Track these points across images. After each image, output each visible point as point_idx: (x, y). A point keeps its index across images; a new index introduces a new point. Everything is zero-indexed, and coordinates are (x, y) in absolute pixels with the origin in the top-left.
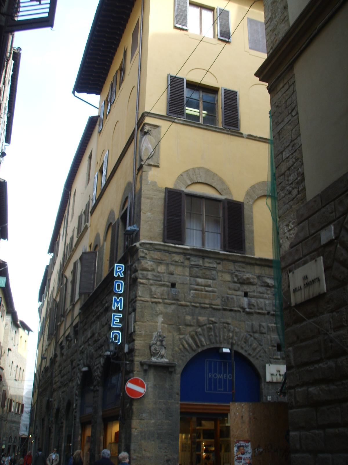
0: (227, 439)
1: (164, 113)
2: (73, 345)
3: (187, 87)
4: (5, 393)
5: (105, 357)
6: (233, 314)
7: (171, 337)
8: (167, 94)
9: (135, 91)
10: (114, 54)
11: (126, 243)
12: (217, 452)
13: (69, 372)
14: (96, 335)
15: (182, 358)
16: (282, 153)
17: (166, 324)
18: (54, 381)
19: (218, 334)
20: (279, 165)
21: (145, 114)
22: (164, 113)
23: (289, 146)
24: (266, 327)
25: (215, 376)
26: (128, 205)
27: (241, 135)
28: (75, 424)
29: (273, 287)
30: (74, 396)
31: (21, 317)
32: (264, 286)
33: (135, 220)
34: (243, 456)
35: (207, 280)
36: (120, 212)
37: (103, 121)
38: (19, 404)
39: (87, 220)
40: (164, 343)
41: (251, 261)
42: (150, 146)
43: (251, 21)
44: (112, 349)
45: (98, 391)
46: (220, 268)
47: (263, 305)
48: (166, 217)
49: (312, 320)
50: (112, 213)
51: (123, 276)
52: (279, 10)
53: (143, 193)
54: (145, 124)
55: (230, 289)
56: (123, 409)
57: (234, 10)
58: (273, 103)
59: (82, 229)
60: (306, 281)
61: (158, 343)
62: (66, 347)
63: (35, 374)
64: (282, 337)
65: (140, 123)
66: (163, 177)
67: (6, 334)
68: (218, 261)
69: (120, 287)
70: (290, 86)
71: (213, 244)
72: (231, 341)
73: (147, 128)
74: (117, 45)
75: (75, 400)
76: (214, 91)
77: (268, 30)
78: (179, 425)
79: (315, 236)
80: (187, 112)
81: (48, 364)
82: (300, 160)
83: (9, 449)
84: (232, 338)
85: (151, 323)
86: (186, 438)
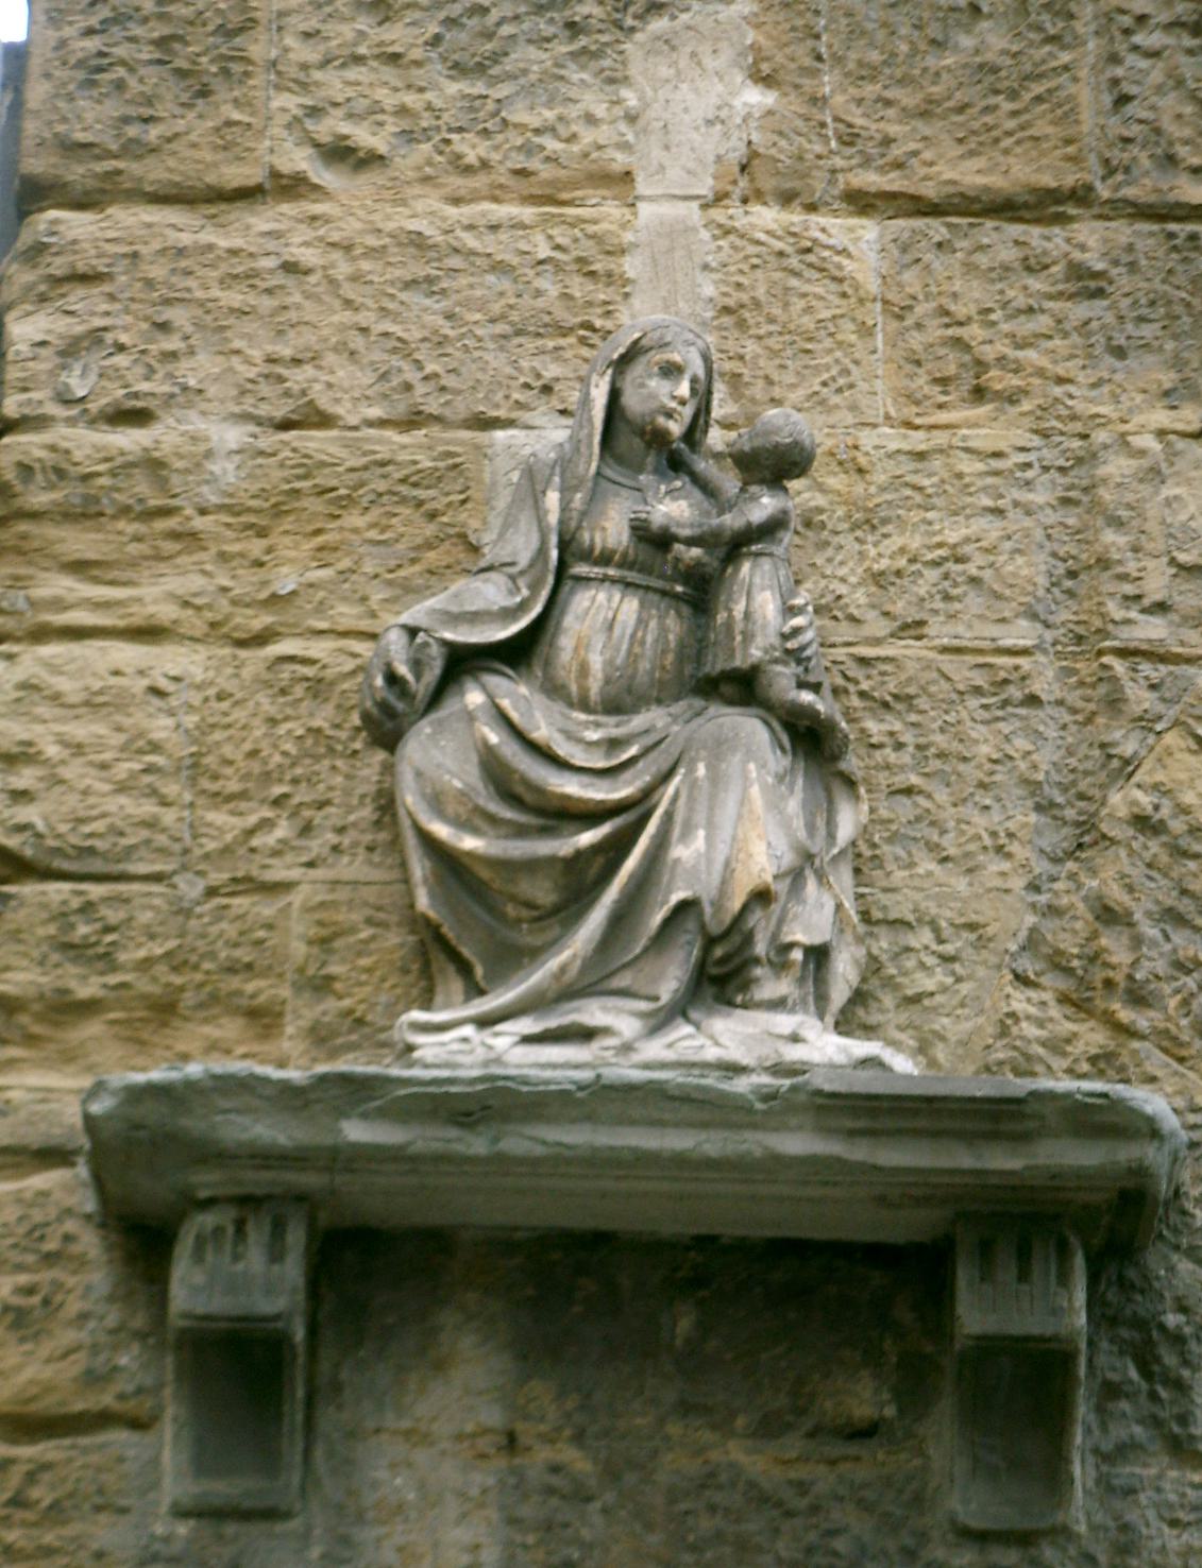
17: (862, 203)
40: (759, 602)
44: (548, 884)
61: (604, 624)
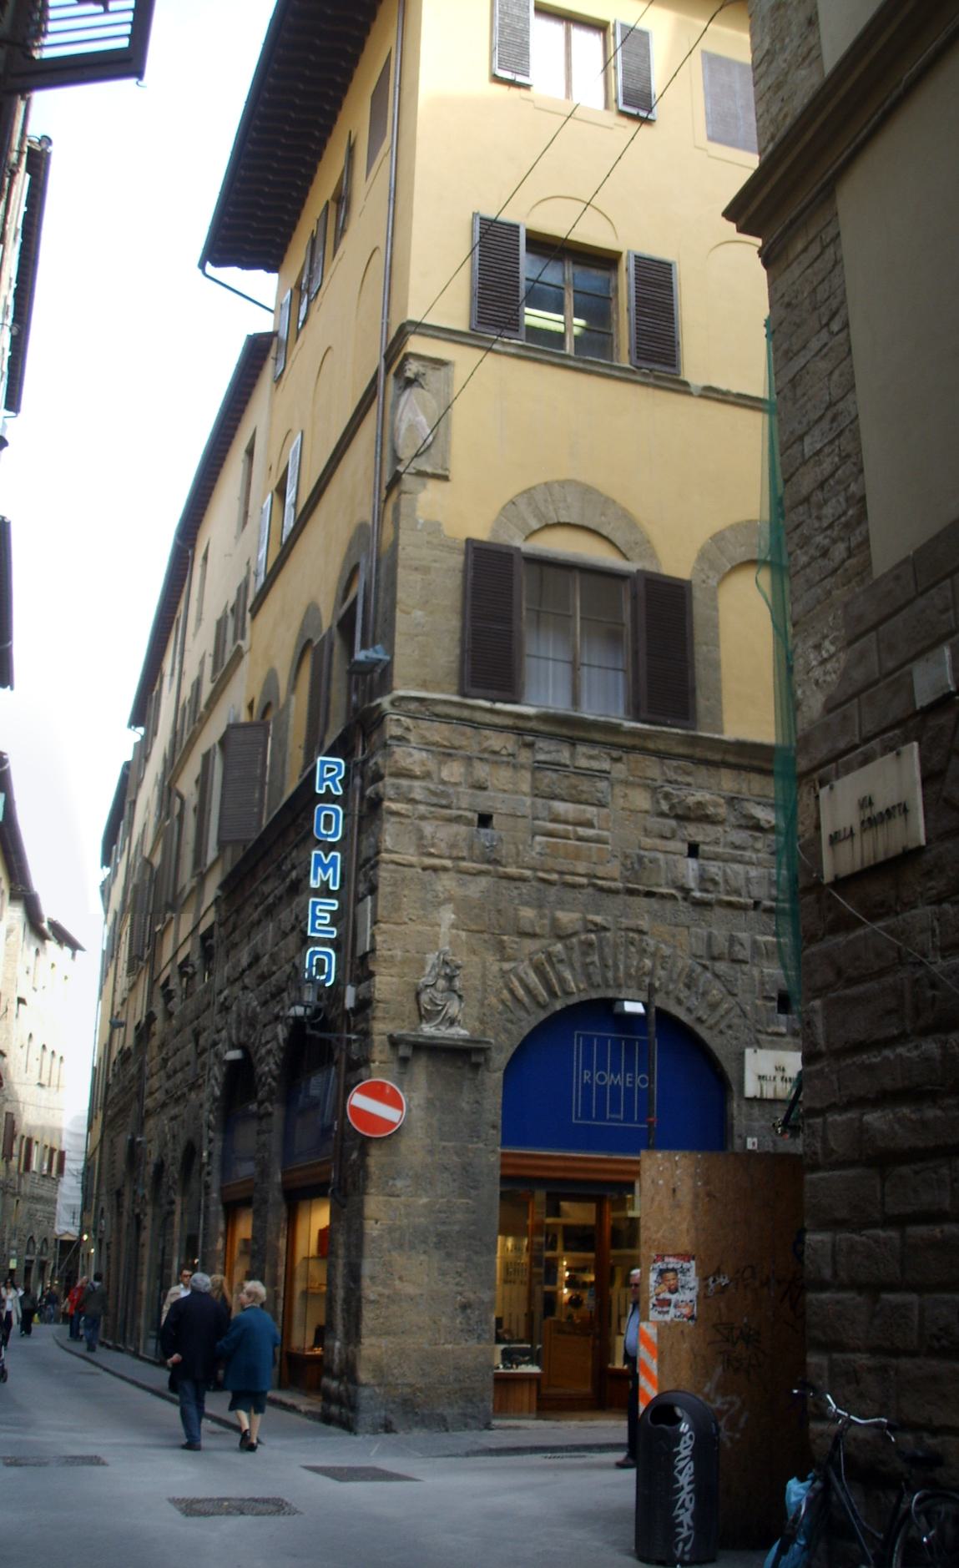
0: (628, 1252)
1: (461, 323)
2: (200, 987)
3: (528, 250)
4: (11, 1122)
5: (291, 1021)
6: (654, 903)
7: (479, 966)
8: (472, 271)
9: (379, 261)
10: (318, 155)
11: (354, 698)
12: (601, 1289)
13: (188, 1064)
14: (265, 959)
15: (509, 1026)
16: (801, 438)
18: (146, 1087)
19: (610, 962)
20: (792, 475)
21: (409, 328)
22: (461, 323)
23: (821, 418)
24: (748, 944)
25: (602, 1078)
26: (358, 588)
27: (683, 388)
28: (207, 1207)
29: (773, 829)
30: (205, 1129)
31: (49, 911)
32: (747, 828)
33: (379, 631)
34: (674, 1297)
35: (583, 807)
36: (335, 610)
37: (285, 347)
38: (52, 1150)
39: (240, 633)
40: (457, 983)
41: (710, 756)
42: (422, 419)
43: (713, 62)
45: (270, 1115)
46: (619, 770)
47: (741, 882)
48: (468, 624)
49: (881, 924)
50: (312, 611)
51: (340, 793)
52: (794, 29)
53: (401, 554)
54: (407, 356)
55: (647, 832)
56: (338, 1167)
57: (664, 30)
58: (779, 295)
59: (228, 657)
60: (868, 813)
61: (442, 983)
62: (179, 993)
63: (94, 1069)
64: (792, 973)
65: (394, 352)
66: (461, 507)
67: (10, 957)
68: (615, 754)
69: (330, 823)
70: (824, 248)
71: (605, 700)
72: (647, 980)
73: (413, 368)
74: (328, 131)
75: (205, 1141)
76: (606, 260)
77: (763, 85)
78: (497, 1211)
79: (898, 678)
80: (528, 320)
81: (130, 1042)
82: (853, 460)
83: (28, 1270)
84: (651, 973)
85: (420, 928)
86: (517, 1248)
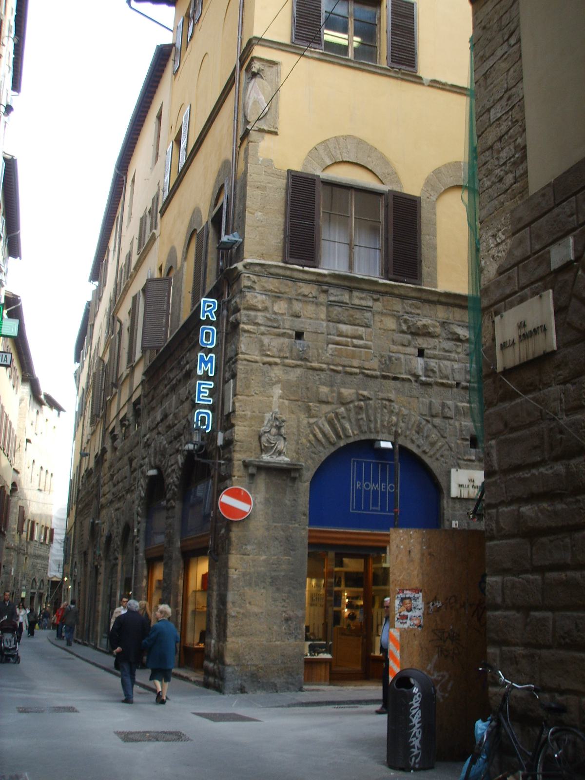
17: (287, 399)
40: (283, 431)
61: (274, 431)
